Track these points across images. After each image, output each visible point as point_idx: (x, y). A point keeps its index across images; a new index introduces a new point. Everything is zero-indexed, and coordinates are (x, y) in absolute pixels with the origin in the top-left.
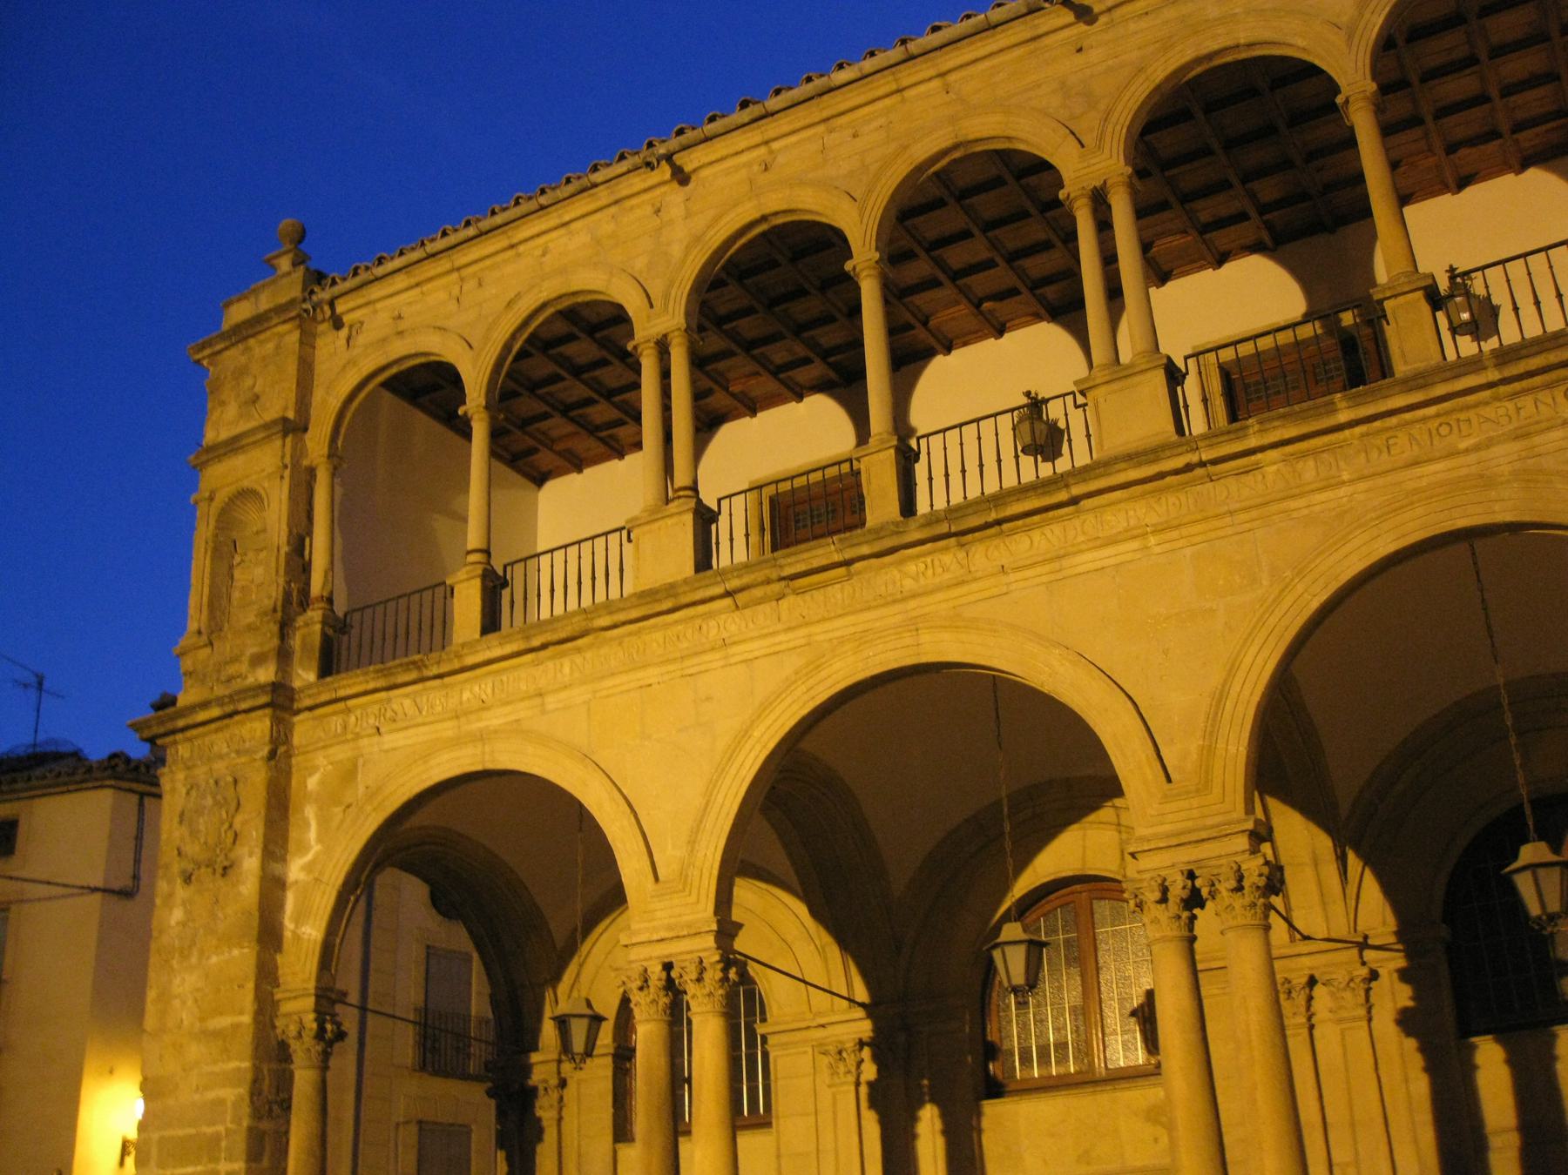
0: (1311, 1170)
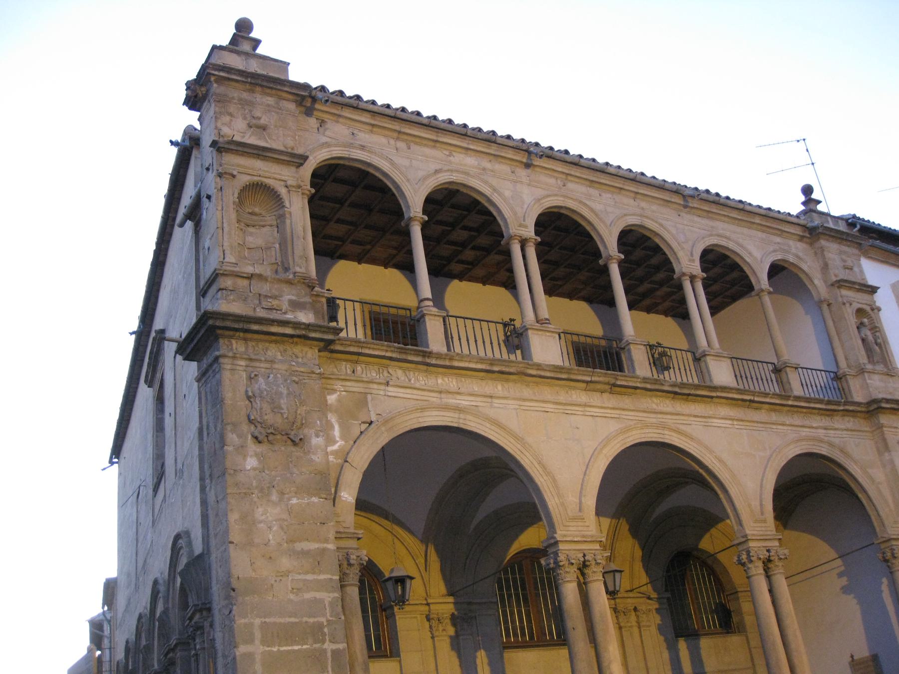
0: (798, 670)
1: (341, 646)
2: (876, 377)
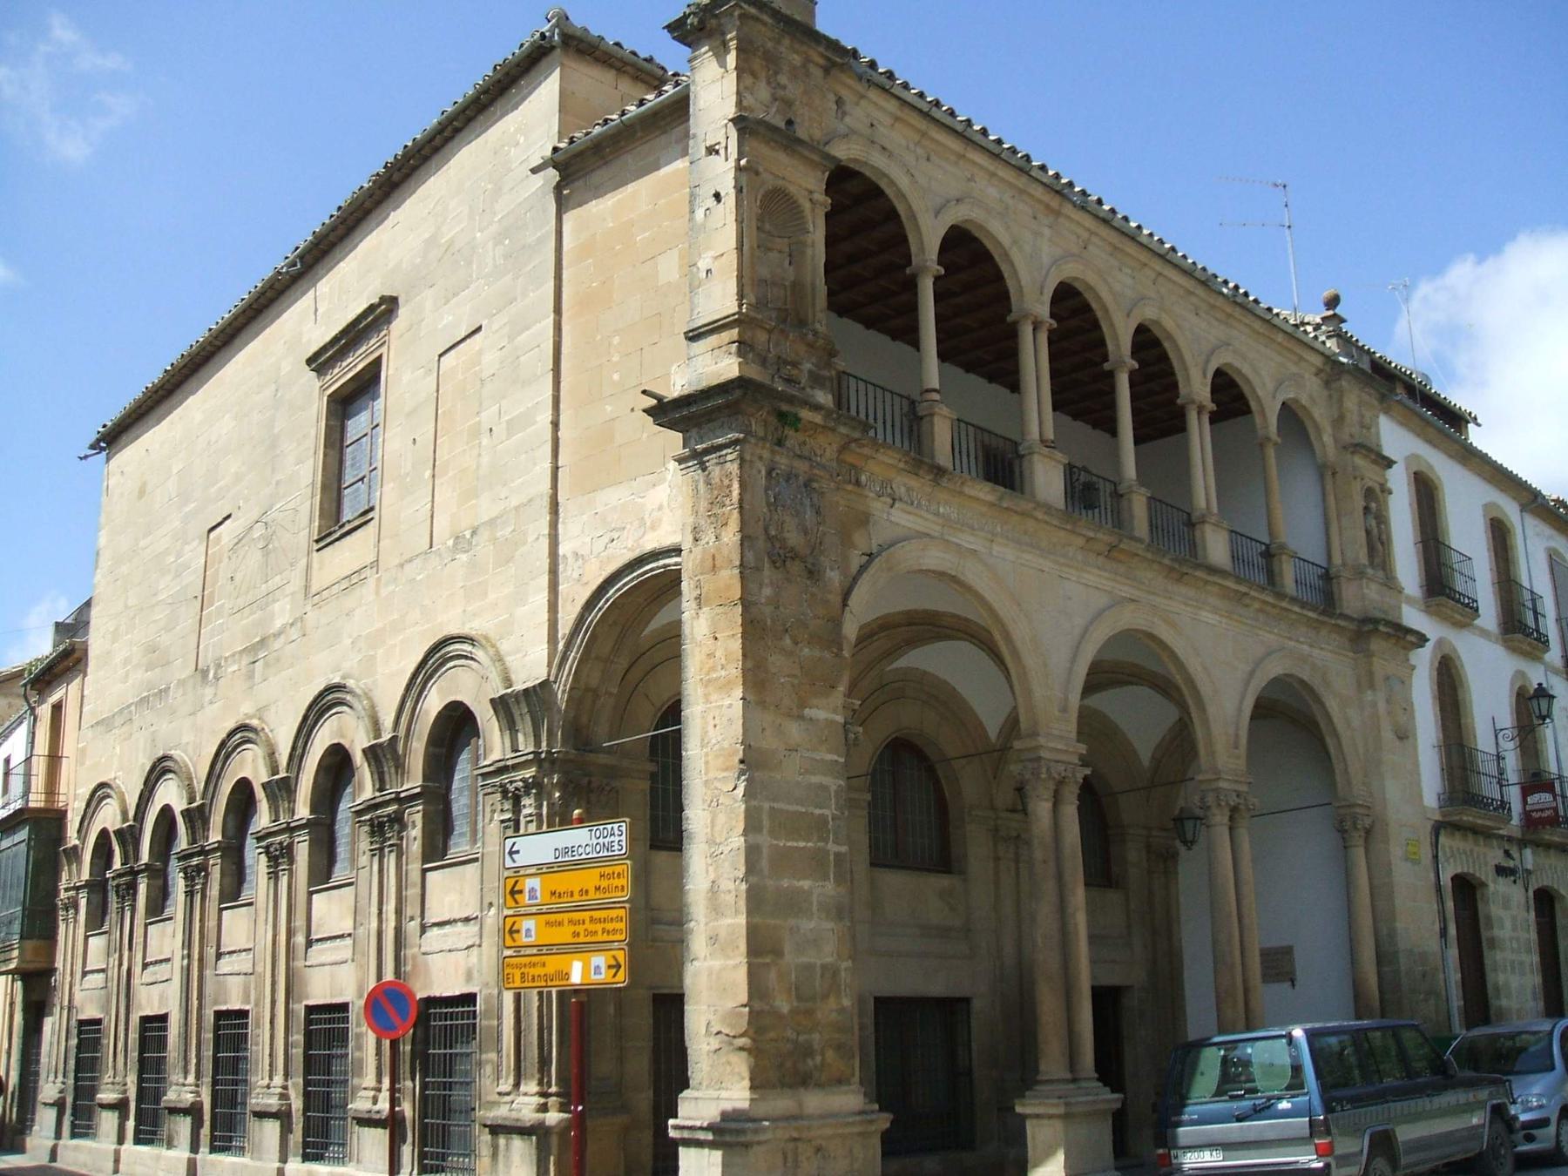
1: (844, 849)
2: (1374, 586)
